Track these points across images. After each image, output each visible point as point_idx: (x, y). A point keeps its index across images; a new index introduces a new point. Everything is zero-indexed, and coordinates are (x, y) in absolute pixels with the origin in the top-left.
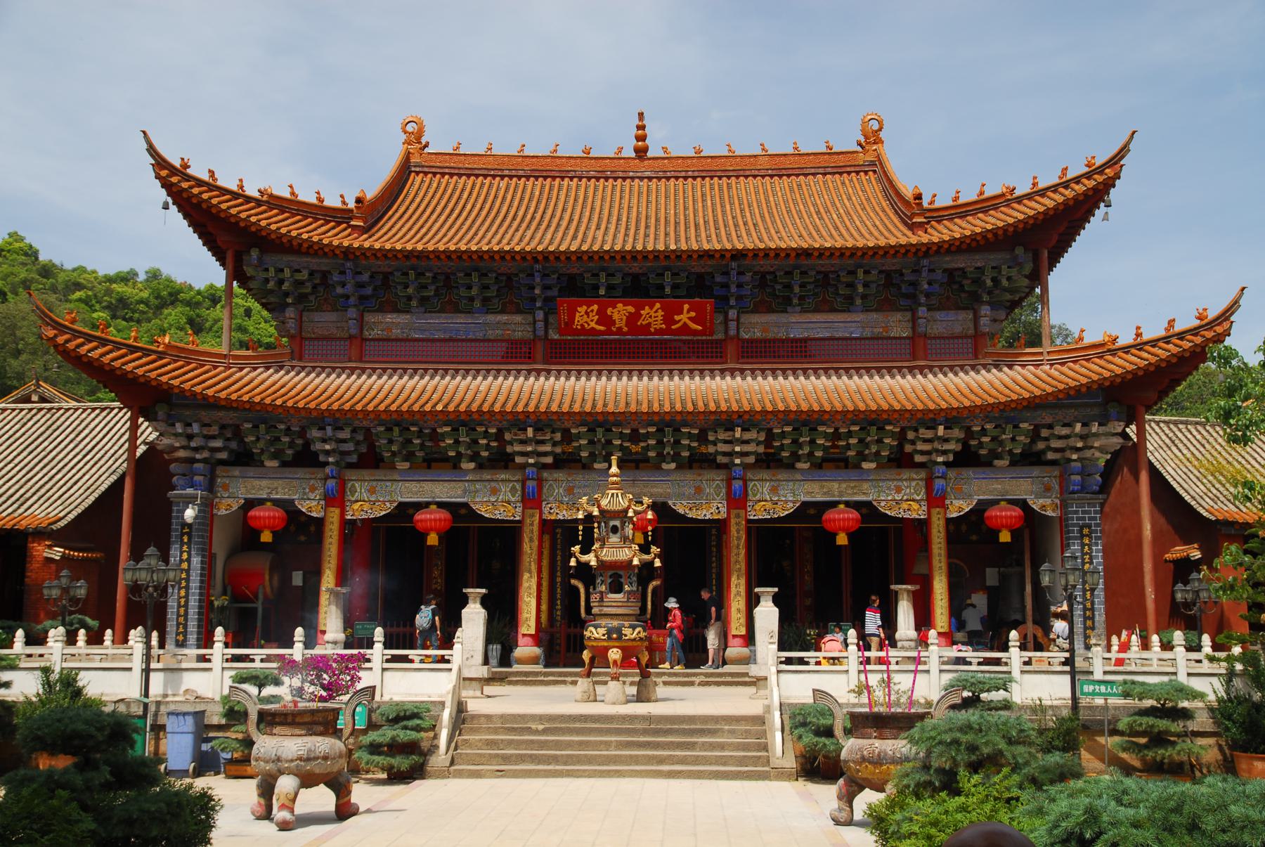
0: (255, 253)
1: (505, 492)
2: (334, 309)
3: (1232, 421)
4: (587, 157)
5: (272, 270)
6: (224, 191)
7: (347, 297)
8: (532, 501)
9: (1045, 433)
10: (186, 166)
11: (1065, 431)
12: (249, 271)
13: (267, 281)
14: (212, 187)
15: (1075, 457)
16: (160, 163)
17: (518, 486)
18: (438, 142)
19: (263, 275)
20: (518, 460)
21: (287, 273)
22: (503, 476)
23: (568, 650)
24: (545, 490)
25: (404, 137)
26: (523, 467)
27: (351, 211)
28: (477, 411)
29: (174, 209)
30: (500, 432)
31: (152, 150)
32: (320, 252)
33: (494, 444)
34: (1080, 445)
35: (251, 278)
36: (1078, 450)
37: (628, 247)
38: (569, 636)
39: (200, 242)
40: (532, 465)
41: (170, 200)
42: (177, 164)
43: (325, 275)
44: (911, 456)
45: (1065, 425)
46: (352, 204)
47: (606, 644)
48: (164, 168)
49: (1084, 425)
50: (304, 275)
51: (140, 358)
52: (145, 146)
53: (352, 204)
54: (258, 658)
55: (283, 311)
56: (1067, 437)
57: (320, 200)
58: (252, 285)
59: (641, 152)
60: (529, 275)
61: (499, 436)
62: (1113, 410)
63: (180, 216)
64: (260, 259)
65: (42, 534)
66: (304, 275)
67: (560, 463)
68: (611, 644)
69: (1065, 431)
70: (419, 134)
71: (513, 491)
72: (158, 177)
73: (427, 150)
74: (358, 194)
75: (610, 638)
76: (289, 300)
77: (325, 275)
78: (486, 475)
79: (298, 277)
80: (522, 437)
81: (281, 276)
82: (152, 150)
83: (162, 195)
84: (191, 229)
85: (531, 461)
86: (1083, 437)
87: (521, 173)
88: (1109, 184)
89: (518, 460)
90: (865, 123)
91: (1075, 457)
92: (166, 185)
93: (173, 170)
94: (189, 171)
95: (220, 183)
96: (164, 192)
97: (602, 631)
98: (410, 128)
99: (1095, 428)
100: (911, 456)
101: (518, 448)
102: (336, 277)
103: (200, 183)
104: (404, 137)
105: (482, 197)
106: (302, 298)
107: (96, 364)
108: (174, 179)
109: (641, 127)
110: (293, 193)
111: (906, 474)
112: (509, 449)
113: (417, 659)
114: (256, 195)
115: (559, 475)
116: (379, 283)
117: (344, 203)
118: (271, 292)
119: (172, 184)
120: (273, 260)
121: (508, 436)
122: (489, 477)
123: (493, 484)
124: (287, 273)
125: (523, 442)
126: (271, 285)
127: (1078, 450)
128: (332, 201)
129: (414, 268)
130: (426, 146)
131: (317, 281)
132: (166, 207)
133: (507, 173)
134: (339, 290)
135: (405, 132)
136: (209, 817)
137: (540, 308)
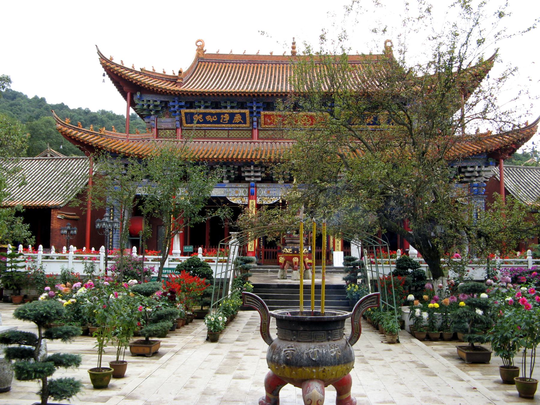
0: (138, 94)
1: (241, 192)
2: (170, 117)
3: (6, 143)
4: (271, 56)
5: (145, 101)
6: (127, 69)
7: (175, 112)
8: (251, 195)
9: (463, 170)
10: (112, 59)
11: (471, 169)
12: (136, 101)
13: (143, 105)
14: (122, 67)
15: (475, 180)
16: (102, 58)
17: (247, 190)
18: (210, 49)
19: (141, 103)
20: (247, 179)
21: (151, 102)
22: (240, 186)
23: (265, 258)
24: (258, 192)
25: (196, 47)
26: (248, 182)
27: (177, 77)
28: (231, 158)
29: (107, 76)
30: (239, 168)
31: (99, 53)
32: (165, 93)
33: (237, 172)
34: (477, 175)
35: (137, 104)
36: (476, 177)
37: (262, 90)
38: (265, 253)
39: (117, 90)
40: (253, 181)
41: (105, 73)
42: (109, 58)
43: (166, 103)
44: (244, 177)
45: (471, 167)
46: (177, 74)
47: (291, 255)
48: (104, 60)
49: (479, 167)
50: (158, 103)
51: (94, 137)
52: (97, 51)
53: (177, 74)
54: (150, 260)
55: (150, 118)
56: (472, 172)
57: (164, 72)
58: (137, 107)
59: (294, 53)
60: (251, 102)
61: (239, 169)
62: (491, 161)
63: (109, 79)
64: (141, 96)
65: (56, 208)
66: (158, 103)
67: (263, 181)
68: (294, 255)
69: (471, 169)
70: (203, 46)
71: (245, 191)
72: (101, 63)
73: (205, 53)
74: (179, 70)
75: (293, 253)
76: (152, 113)
77: (166, 103)
78: (233, 185)
79: (156, 103)
80: (249, 169)
81: (149, 103)
82: (99, 53)
83: (103, 71)
84: (113, 84)
85: (252, 179)
86: (479, 172)
87: (244, 62)
88: (487, 71)
89: (247, 179)
90: (385, 43)
91: (475, 180)
92: (105, 67)
93: (108, 61)
94: (113, 61)
95: (125, 66)
96: (103, 69)
97: (290, 250)
98: (199, 44)
99: (483, 168)
100: (244, 177)
101: (246, 174)
102: (171, 104)
103: (117, 66)
104: (196, 47)
105: (250, 77)
106: (157, 112)
107: (77, 139)
108: (108, 64)
109: (294, 43)
110: (154, 70)
111: (240, 185)
112: (243, 175)
113: (216, 261)
114: (140, 70)
115: (263, 185)
116: (163, 105)
117: (174, 74)
118: (145, 110)
119: (107, 66)
120: (146, 97)
121: (242, 169)
122: (235, 186)
123: (236, 189)
124: (151, 102)
125: (249, 172)
126: (145, 106)
127: (476, 177)
128: (169, 73)
129: (203, 100)
130: (205, 51)
131: (163, 105)
132: (104, 75)
133: (238, 62)
134: (172, 109)
135: (197, 45)
136: (67, 338)
137: (255, 116)
